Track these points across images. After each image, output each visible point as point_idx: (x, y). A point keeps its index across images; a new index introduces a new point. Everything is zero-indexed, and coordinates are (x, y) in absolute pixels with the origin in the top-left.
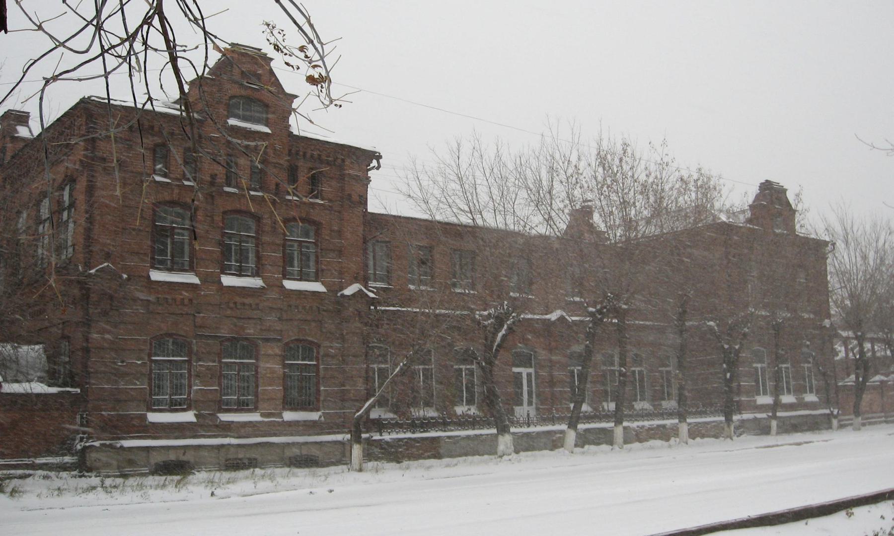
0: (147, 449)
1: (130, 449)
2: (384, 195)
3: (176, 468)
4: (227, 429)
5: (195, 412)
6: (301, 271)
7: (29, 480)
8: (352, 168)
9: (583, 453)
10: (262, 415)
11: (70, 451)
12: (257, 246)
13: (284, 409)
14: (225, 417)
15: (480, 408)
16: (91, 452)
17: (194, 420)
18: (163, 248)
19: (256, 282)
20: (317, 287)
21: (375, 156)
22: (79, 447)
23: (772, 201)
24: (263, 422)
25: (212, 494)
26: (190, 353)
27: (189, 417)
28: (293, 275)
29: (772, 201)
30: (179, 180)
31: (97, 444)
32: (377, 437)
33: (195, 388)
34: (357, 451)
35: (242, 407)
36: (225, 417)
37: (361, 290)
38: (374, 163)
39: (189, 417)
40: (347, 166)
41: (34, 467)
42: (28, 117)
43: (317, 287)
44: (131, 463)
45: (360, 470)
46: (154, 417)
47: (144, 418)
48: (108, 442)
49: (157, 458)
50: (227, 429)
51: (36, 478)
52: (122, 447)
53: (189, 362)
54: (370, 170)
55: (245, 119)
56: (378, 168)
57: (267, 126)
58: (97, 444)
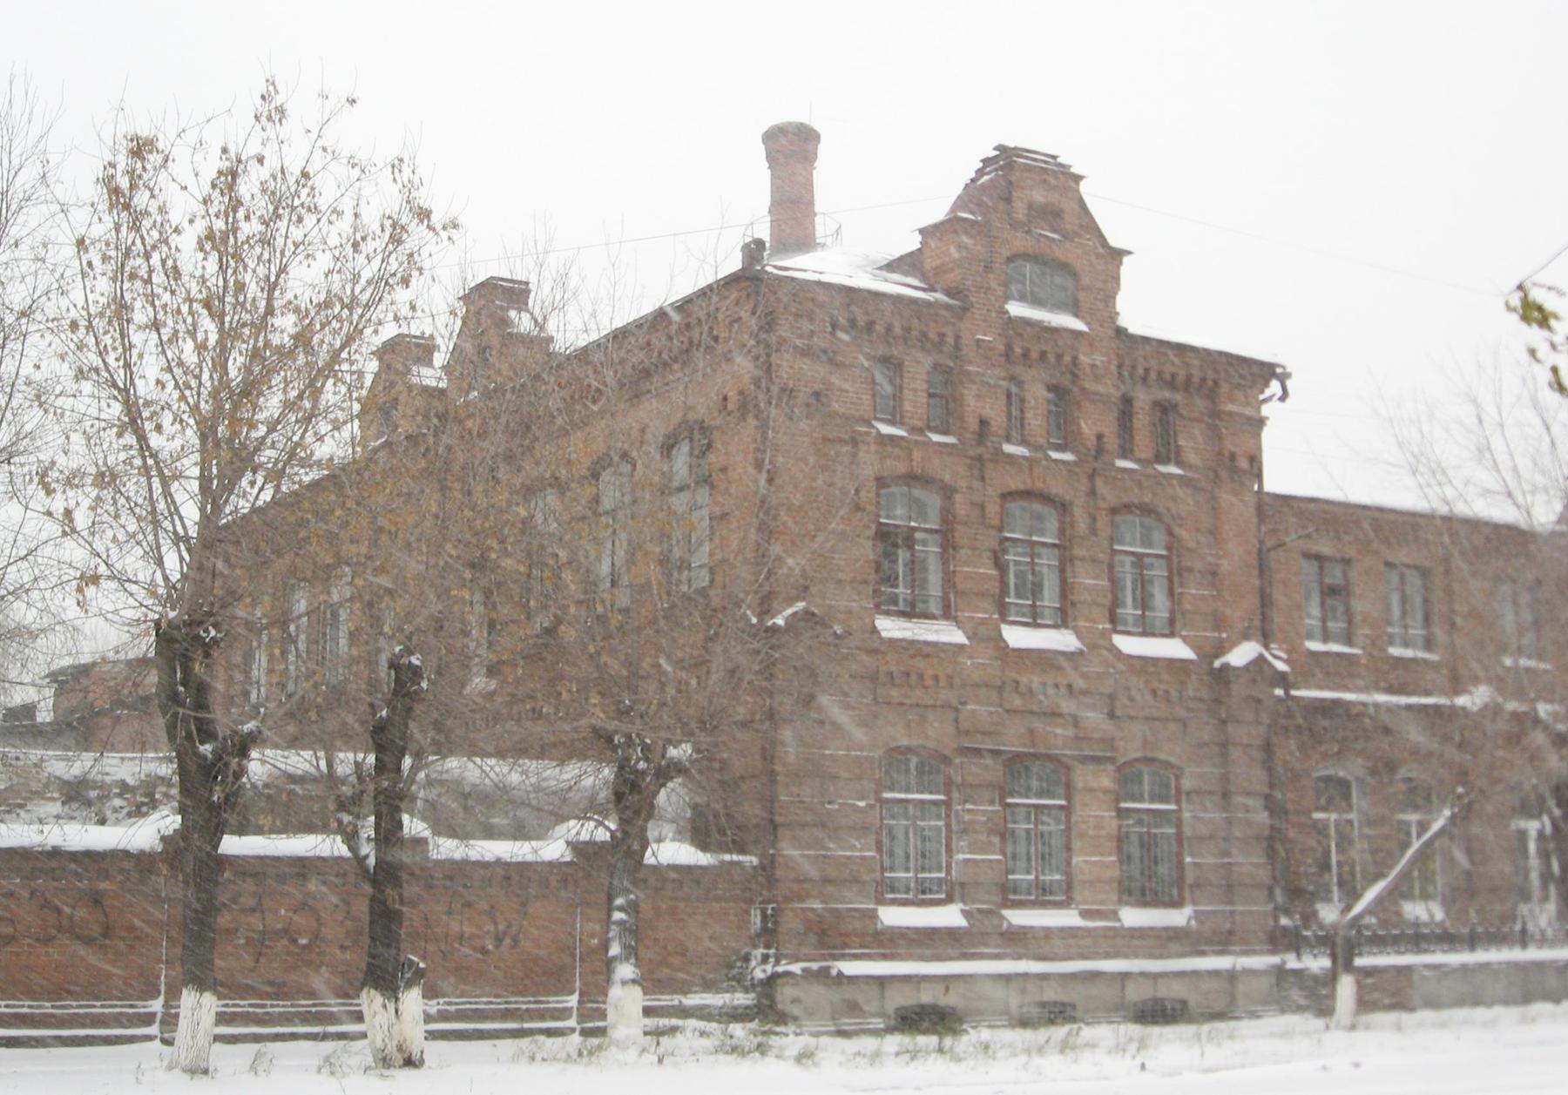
0: (881, 981)
1: (853, 979)
2: (1301, 455)
3: (929, 1019)
4: (1019, 941)
5: (961, 906)
6: (1143, 615)
7: (679, 1039)
8: (1232, 400)
9: (1443, 1025)
10: (1085, 914)
11: (740, 983)
12: (945, 548)
13: (1121, 902)
14: (1019, 918)
15: (1447, 905)
16: (784, 984)
17: (961, 922)
18: (891, 567)
19: (1062, 640)
20: (1175, 649)
21: (1265, 372)
22: (759, 974)
23: (1025, 213)
24: (1088, 930)
25: (1143, 1067)
26: (948, 786)
27: (950, 916)
28: (1126, 624)
29: (1025, 213)
30: (920, 431)
31: (796, 968)
32: (1292, 962)
33: (961, 856)
34: (1346, 988)
35: (1043, 897)
36: (1019, 918)
37: (1261, 658)
38: (1275, 387)
39: (950, 916)
40: (1215, 393)
41: (684, 1012)
42: (528, 292)
43: (1175, 649)
44: (854, 1008)
45: (1353, 1027)
46: (893, 916)
47: (873, 915)
48: (815, 966)
49: (899, 998)
50: (1019, 941)
51: (689, 1034)
52: (840, 974)
53: (948, 804)
54: (1265, 401)
55: (1036, 302)
56: (1283, 398)
57: (1076, 315)
58: (796, 968)
